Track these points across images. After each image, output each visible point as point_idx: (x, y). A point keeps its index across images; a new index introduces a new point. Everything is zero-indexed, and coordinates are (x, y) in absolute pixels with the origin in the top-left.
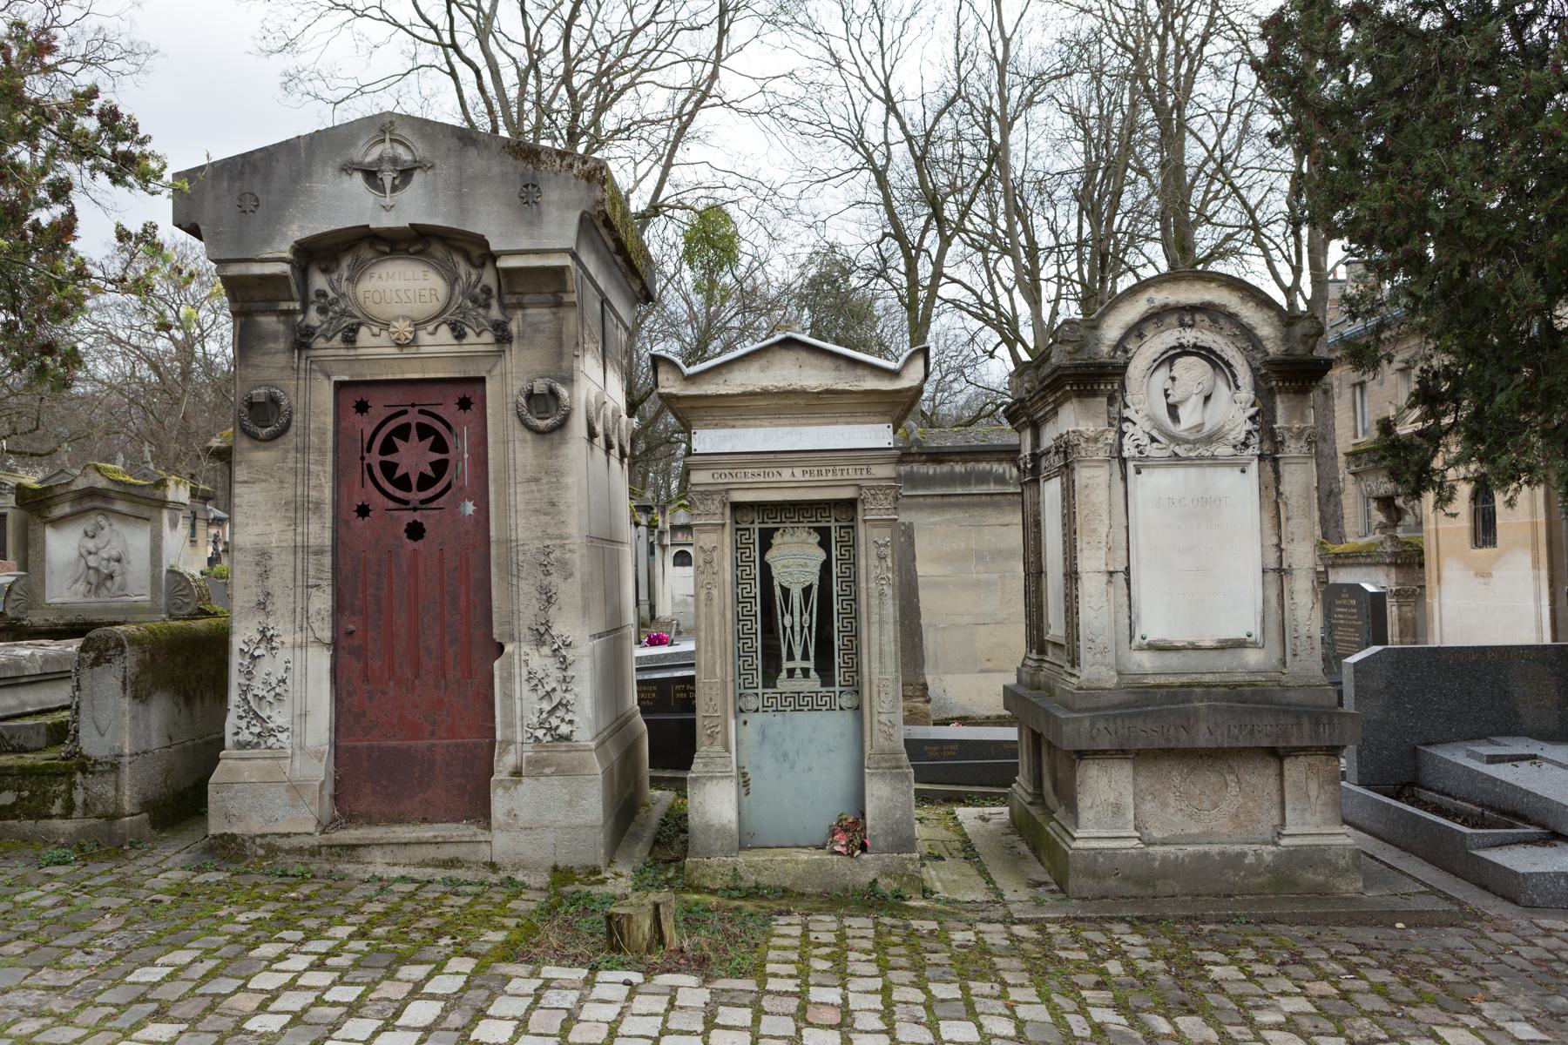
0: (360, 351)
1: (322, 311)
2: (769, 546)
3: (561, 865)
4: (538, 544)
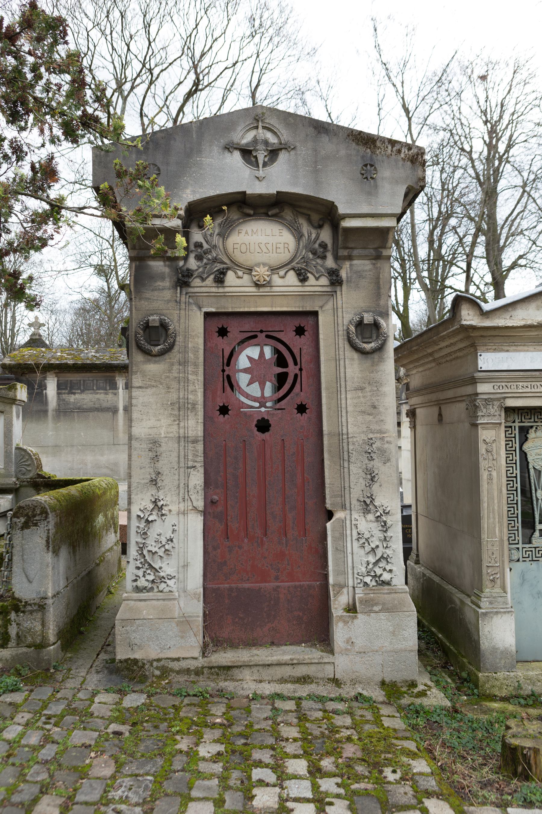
0: (227, 289)
1: (199, 258)
2: (526, 439)
3: (387, 680)
4: (364, 437)
